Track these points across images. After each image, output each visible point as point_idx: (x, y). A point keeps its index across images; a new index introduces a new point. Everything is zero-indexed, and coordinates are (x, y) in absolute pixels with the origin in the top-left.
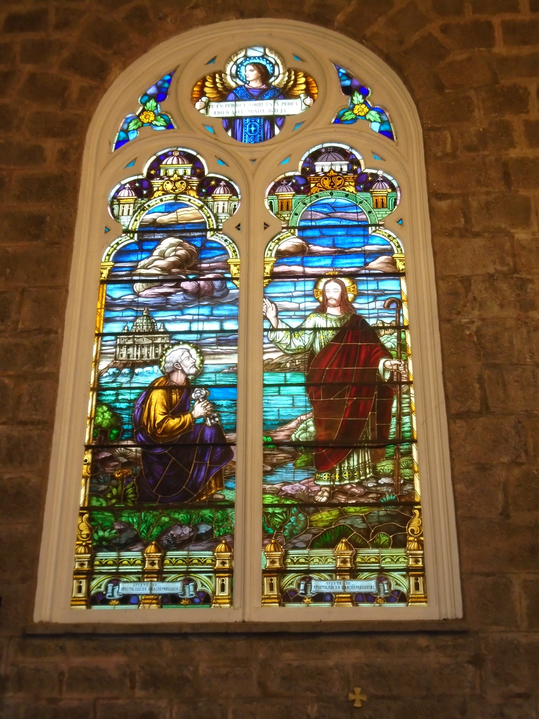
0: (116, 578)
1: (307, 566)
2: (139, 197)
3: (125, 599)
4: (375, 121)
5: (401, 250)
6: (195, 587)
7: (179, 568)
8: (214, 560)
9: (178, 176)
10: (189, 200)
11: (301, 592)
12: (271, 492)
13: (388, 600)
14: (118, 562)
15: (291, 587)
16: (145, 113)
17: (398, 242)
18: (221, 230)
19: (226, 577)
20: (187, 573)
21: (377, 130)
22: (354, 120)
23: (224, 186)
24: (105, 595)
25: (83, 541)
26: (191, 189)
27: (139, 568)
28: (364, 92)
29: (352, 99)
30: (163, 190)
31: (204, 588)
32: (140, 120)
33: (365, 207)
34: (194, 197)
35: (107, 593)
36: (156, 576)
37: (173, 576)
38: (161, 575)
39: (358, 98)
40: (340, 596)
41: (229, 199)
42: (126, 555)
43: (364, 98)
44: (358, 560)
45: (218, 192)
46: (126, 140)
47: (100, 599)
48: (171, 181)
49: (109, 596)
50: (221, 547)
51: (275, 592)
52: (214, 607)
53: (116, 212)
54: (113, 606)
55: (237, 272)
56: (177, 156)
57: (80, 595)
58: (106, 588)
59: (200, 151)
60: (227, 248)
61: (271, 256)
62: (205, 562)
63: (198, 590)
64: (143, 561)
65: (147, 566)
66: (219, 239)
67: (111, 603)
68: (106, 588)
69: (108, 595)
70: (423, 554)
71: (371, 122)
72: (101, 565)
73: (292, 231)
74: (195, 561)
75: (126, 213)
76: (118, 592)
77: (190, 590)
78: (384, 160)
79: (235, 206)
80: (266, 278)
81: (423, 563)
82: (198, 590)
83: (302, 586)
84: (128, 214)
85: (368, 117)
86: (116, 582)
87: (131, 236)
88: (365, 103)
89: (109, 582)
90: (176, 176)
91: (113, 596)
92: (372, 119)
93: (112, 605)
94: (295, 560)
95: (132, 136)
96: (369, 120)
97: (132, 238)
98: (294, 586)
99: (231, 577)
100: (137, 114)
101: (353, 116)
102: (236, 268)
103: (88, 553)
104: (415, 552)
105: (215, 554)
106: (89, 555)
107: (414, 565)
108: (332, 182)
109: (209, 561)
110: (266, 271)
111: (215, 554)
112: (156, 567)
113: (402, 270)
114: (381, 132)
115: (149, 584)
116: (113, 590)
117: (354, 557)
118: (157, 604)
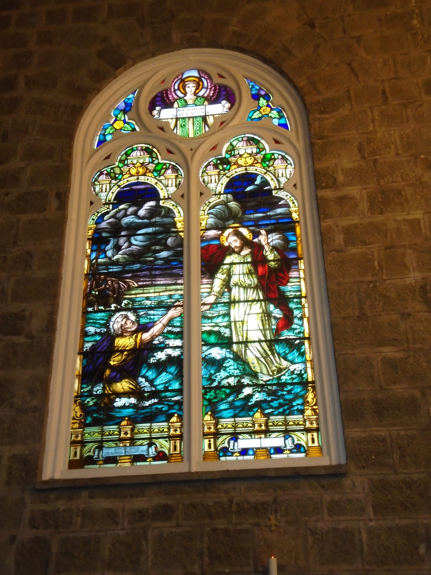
0: (235, 436)
1: (252, 429)
2: (112, 179)
3: (244, 452)
4: (275, 118)
5: (180, 215)
6: (156, 447)
7: (226, 431)
8: (169, 429)
9: (140, 164)
10: (148, 179)
11: (95, 457)
12: (162, 382)
13: (155, 459)
14: (286, 423)
15: (223, 446)
16: (117, 122)
17: (178, 210)
18: (282, 189)
19: (178, 440)
20: (150, 439)
21: (277, 124)
22: (260, 118)
23: (281, 158)
24: (228, 449)
25: (78, 420)
26: (258, 162)
27: (302, 427)
28: (267, 97)
29: (259, 103)
30: (130, 174)
31: (299, 442)
32: (114, 127)
33: (160, 187)
34: (151, 177)
35: (94, 456)
36: (213, 436)
37: (276, 434)
38: (267, 432)
39: (263, 102)
40: (122, 458)
41: (286, 167)
42: (156, 426)
43: (268, 101)
44: (220, 426)
45: (277, 163)
46: (105, 140)
47: (90, 461)
48: (135, 167)
49: (231, 449)
50: (174, 419)
51: (213, 449)
52: (120, 465)
53: (97, 190)
54: (149, 463)
55: (181, 226)
56: (140, 150)
57: (313, 445)
58: (229, 443)
59: (155, 144)
60: (174, 210)
61: (204, 215)
62: (163, 430)
63: (295, 443)
64: (305, 421)
65: (172, 432)
66: (169, 204)
67: (285, 453)
68: (229, 443)
69: (95, 457)
70: (317, 419)
71: (273, 118)
72: (274, 425)
73: (219, 196)
74: (291, 423)
75: (104, 190)
76: (102, 456)
77: (289, 444)
78: (211, 150)
79: (180, 181)
80: (202, 230)
81: (318, 424)
82: (295, 443)
83: (96, 453)
84: (106, 191)
85: (270, 115)
86: (236, 439)
87: (108, 207)
88: (268, 106)
89: (96, 448)
90: (138, 164)
91: (98, 458)
92: (273, 116)
93: (286, 454)
94: (276, 423)
95: (109, 138)
96: (271, 117)
97: (219, 198)
98: (91, 454)
99: (181, 440)
100: (112, 122)
101: (260, 115)
102: (180, 224)
103: (213, 420)
104: (310, 417)
105: (305, 417)
106: (214, 421)
107: (174, 433)
108: (138, 171)
109: (166, 430)
110: (202, 225)
111: (305, 417)
112: (129, 436)
113: (296, 219)
114: (280, 125)
115: (259, 440)
116: (234, 444)
117: (83, 435)
118: (130, 462)
